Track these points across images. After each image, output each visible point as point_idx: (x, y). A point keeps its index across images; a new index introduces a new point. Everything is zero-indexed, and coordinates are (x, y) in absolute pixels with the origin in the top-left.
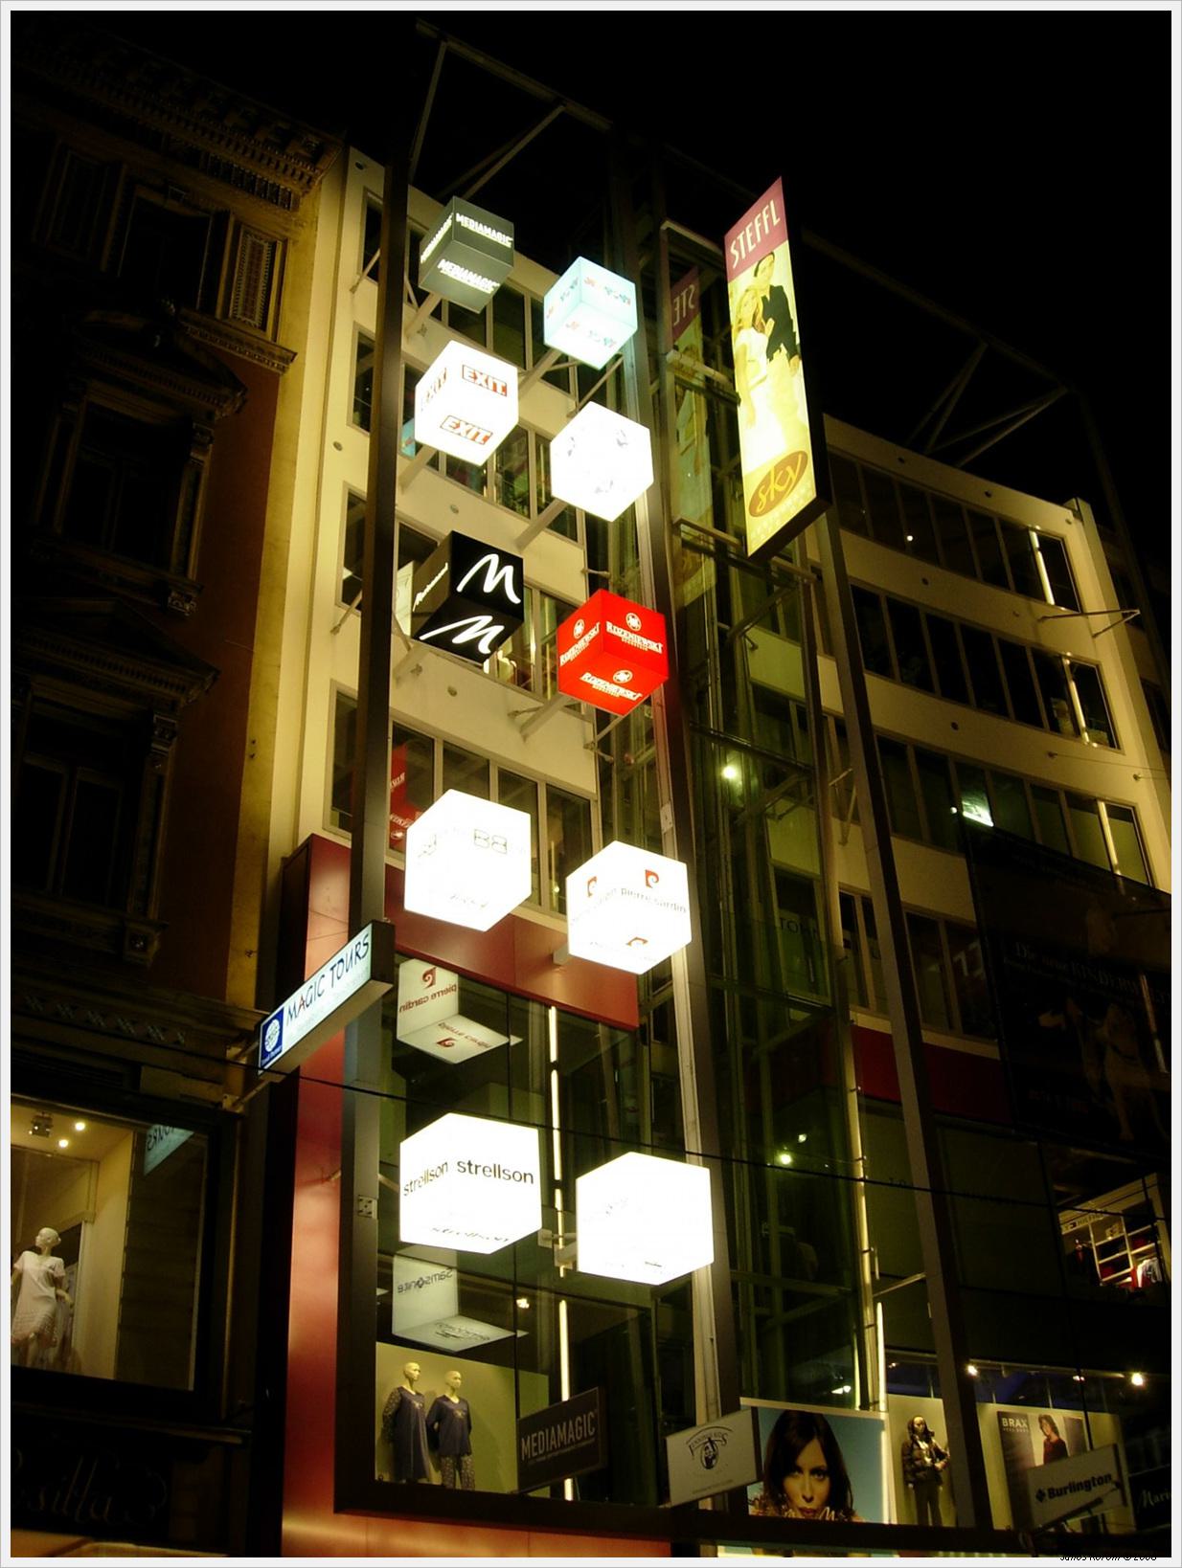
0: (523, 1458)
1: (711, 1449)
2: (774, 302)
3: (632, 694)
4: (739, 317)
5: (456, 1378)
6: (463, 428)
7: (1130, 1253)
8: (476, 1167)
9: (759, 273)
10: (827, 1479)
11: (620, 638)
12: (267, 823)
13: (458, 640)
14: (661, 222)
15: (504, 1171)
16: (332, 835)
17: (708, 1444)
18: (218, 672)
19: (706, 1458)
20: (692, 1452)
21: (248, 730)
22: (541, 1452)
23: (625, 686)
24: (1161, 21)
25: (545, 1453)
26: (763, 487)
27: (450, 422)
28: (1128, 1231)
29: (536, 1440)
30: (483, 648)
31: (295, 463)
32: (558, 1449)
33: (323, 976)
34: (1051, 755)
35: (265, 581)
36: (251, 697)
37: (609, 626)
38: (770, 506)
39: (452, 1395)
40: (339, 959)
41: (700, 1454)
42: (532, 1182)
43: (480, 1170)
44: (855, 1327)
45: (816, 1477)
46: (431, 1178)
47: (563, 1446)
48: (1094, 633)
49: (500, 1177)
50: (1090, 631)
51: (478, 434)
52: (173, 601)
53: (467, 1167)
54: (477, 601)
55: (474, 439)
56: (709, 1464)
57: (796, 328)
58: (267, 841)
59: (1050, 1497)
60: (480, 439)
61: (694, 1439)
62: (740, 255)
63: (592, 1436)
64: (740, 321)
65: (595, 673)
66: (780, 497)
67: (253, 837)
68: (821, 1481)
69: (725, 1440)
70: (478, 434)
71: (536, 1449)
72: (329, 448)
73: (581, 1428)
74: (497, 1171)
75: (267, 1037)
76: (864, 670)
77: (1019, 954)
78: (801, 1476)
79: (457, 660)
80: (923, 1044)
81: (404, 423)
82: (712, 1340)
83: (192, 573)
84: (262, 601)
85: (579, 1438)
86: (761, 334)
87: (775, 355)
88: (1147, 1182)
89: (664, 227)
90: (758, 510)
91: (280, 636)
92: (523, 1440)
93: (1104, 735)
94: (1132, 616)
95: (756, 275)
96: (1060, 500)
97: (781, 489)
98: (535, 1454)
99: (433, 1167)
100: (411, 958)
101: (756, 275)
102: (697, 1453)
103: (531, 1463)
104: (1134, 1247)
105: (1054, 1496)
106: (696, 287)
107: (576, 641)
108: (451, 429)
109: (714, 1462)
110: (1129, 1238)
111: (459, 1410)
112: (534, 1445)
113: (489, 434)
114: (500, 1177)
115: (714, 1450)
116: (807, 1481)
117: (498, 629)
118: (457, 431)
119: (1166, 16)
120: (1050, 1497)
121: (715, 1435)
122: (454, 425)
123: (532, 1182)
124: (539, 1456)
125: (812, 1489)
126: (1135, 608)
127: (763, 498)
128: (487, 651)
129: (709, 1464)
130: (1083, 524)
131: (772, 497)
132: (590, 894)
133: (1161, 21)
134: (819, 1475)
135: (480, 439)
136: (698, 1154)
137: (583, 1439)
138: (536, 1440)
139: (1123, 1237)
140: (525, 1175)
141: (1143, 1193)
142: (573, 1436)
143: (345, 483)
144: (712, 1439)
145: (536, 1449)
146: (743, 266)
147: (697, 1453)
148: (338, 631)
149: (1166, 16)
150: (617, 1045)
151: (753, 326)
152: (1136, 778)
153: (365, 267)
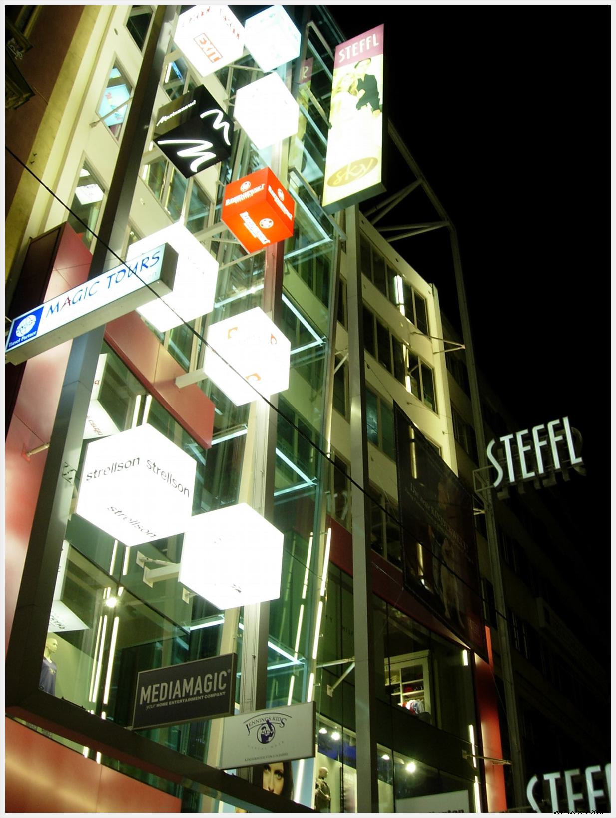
0: (141, 703)
1: (268, 728)
2: (368, 83)
3: (265, 239)
4: (339, 86)
5: (54, 644)
6: (208, 45)
7: (402, 694)
9: (357, 67)
10: (282, 779)
11: (273, 199)
12: (30, 207)
13: (182, 154)
14: (308, 22)
17: (266, 725)
18: (33, 94)
19: (263, 736)
20: (249, 729)
21: (34, 146)
22: (161, 699)
23: (264, 231)
24: (605, 11)
25: (167, 700)
26: (341, 172)
27: (201, 38)
28: (403, 681)
29: (158, 689)
30: (194, 167)
31: (95, 22)
32: (182, 698)
34: (408, 403)
35: (63, 71)
36: (40, 129)
37: (270, 189)
38: (344, 182)
39: (48, 656)
41: (256, 732)
43: (160, 472)
45: (277, 775)
46: (118, 468)
47: (187, 695)
48: (434, 352)
50: (432, 350)
51: (214, 53)
52: (11, 44)
53: (153, 466)
54: (205, 130)
55: (209, 57)
56: (265, 739)
57: (381, 96)
58: (28, 218)
60: (213, 58)
61: (253, 720)
62: (346, 57)
63: (223, 691)
64: (339, 88)
65: (251, 215)
66: (352, 179)
67: (20, 211)
68: (279, 779)
69: (284, 724)
70: (214, 53)
71: (157, 696)
72: (111, 31)
73: (210, 683)
74: (170, 479)
75: (18, 328)
77: (411, 490)
78: (269, 773)
79: (168, 175)
82: (254, 657)
83: (27, 33)
84: (60, 80)
85: (206, 691)
86: (355, 96)
87: (362, 108)
88: (391, 660)
89: (309, 25)
90: (335, 183)
91: (65, 105)
92: (143, 689)
93: (431, 405)
94: (459, 348)
95: (356, 67)
96: (428, 281)
97: (354, 175)
98: (154, 700)
99: (124, 460)
101: (356, 67)
102: (254, 731)
103: (152, 707)
104: (405, 691)
106: (309, 69)
107: (242, 193)
108: (200, 44)
109: (270, 738)
110: (403, 685)
111: (53, 669)
112: (155, 693)
113: (220, 57)
115: (271, 730)
116: (272, 776)
117: (212, 156)
118: (202, 46)
119: (608, 8)
121: (274, 719)
122: (203, 41)
124: (159, 702)
125: (274, 785)
126: (463, 344)
127: (340, 178)
128: (196, 171)
129: (265, 739)
130: (434, 298)
131: (347, 178)
132: (229, 337)
133: (605, 11)
134: (279, 775)
135: (213, 58)
137: (212, 692)
138: (158, 689)
139: (399, 684)
141: (391, 663)
142: (200, 688)
143: (115, 53)
144: (270, 721)
145: (157, 696)
146: (346, 62)
147: (254, 731)
148: (95, 126)
149: (608, 8)
151: (349, 92)
152: (443, 433)
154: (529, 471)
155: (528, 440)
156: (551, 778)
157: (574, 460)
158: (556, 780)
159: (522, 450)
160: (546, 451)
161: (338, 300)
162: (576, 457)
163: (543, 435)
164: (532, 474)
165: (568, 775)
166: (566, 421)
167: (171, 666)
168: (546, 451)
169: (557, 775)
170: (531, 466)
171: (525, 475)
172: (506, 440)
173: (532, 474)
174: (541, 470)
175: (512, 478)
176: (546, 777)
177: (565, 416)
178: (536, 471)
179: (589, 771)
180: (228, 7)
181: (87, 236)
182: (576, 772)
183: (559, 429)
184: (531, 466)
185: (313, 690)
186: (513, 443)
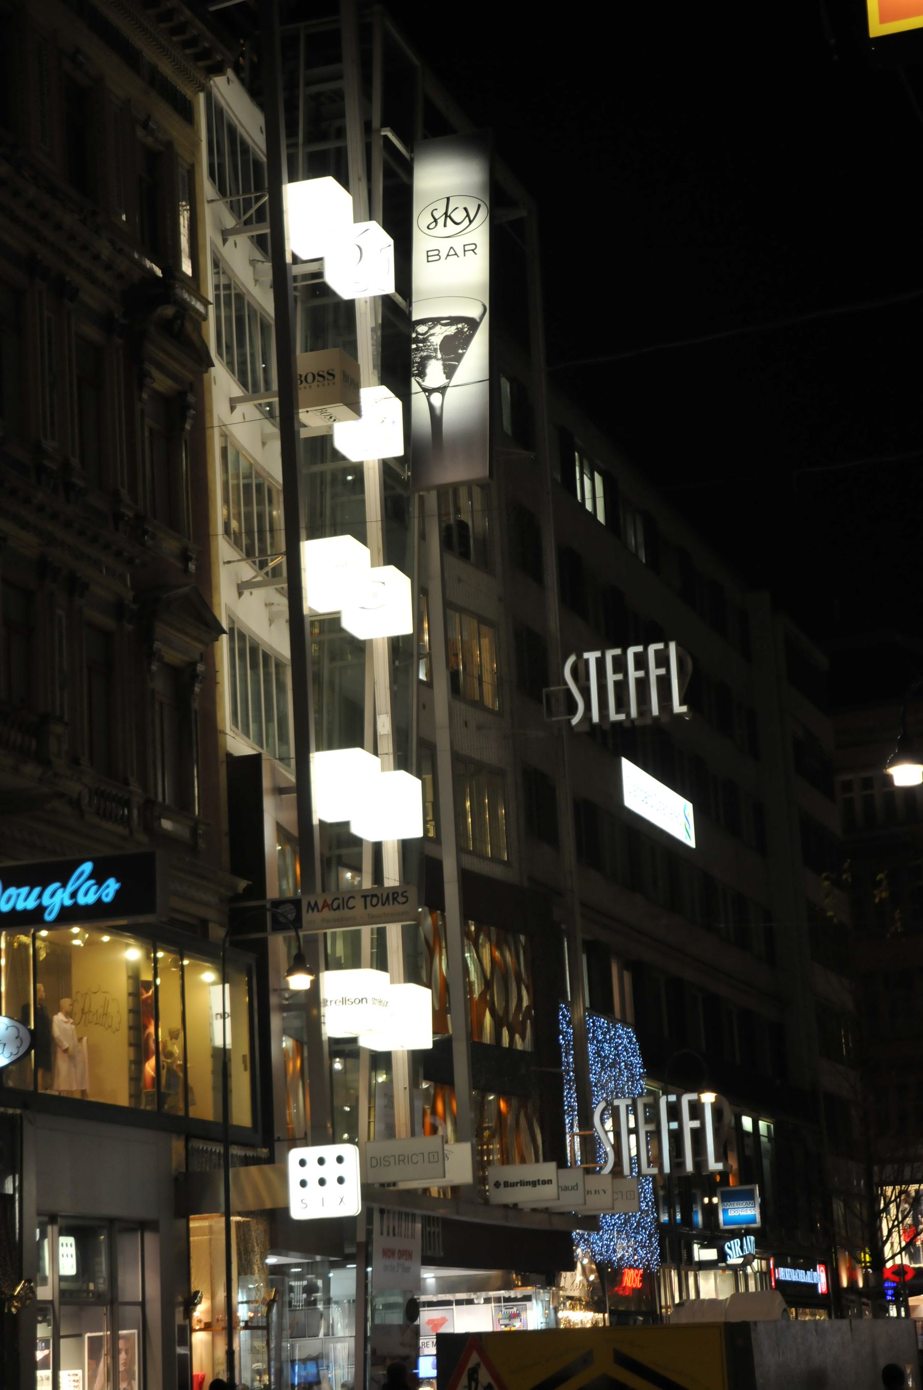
8: (331, 1001)
15: (348, 1000)
16: (232, 732)
33: (72, 1267)
40: (76, 1373)
42: (367, 1002)
44: (833, 1250)
49: (346, 1004)
59: (505, 1186)
76: (177, 1344)
80: (60, 1339)
81: (224, 244)
100: (388, 226)
105: (508, 1186)
114: (346, 1004)
120: (505, 1186)
123: (367, 1002)
136: (488, 683)
140: (362, 999)
150: (448, 386)
153: (215, 183)
154: (618, 711)
155: (620, 665)
156: (591, 657)
157: (678, 708)
158: (597, 659)
159: (612, 678)
160: (642, 684)
161: (429, 805)
162: (681, 704)
163: (641, 661)
164: (622, 717)
165: (610, 654)
166: (672, 646)
167: (293, 762)
168: (642, 684)
169: (598, 654)
170: (622, 705)
171: (614, 716)
172: (591, 657)
173: (622, 717)
174: (634, 713)
175: (596, 718)
176: (586, 655)
177: (672, 640)
178: (628, 715)
179: (632, 651)
180: (233, 413)
181: (269, 1256)
182: (618, 651)
183: (662, 659)
184: (622, 705)
185: (460, 1270)
186: (601, 663)
